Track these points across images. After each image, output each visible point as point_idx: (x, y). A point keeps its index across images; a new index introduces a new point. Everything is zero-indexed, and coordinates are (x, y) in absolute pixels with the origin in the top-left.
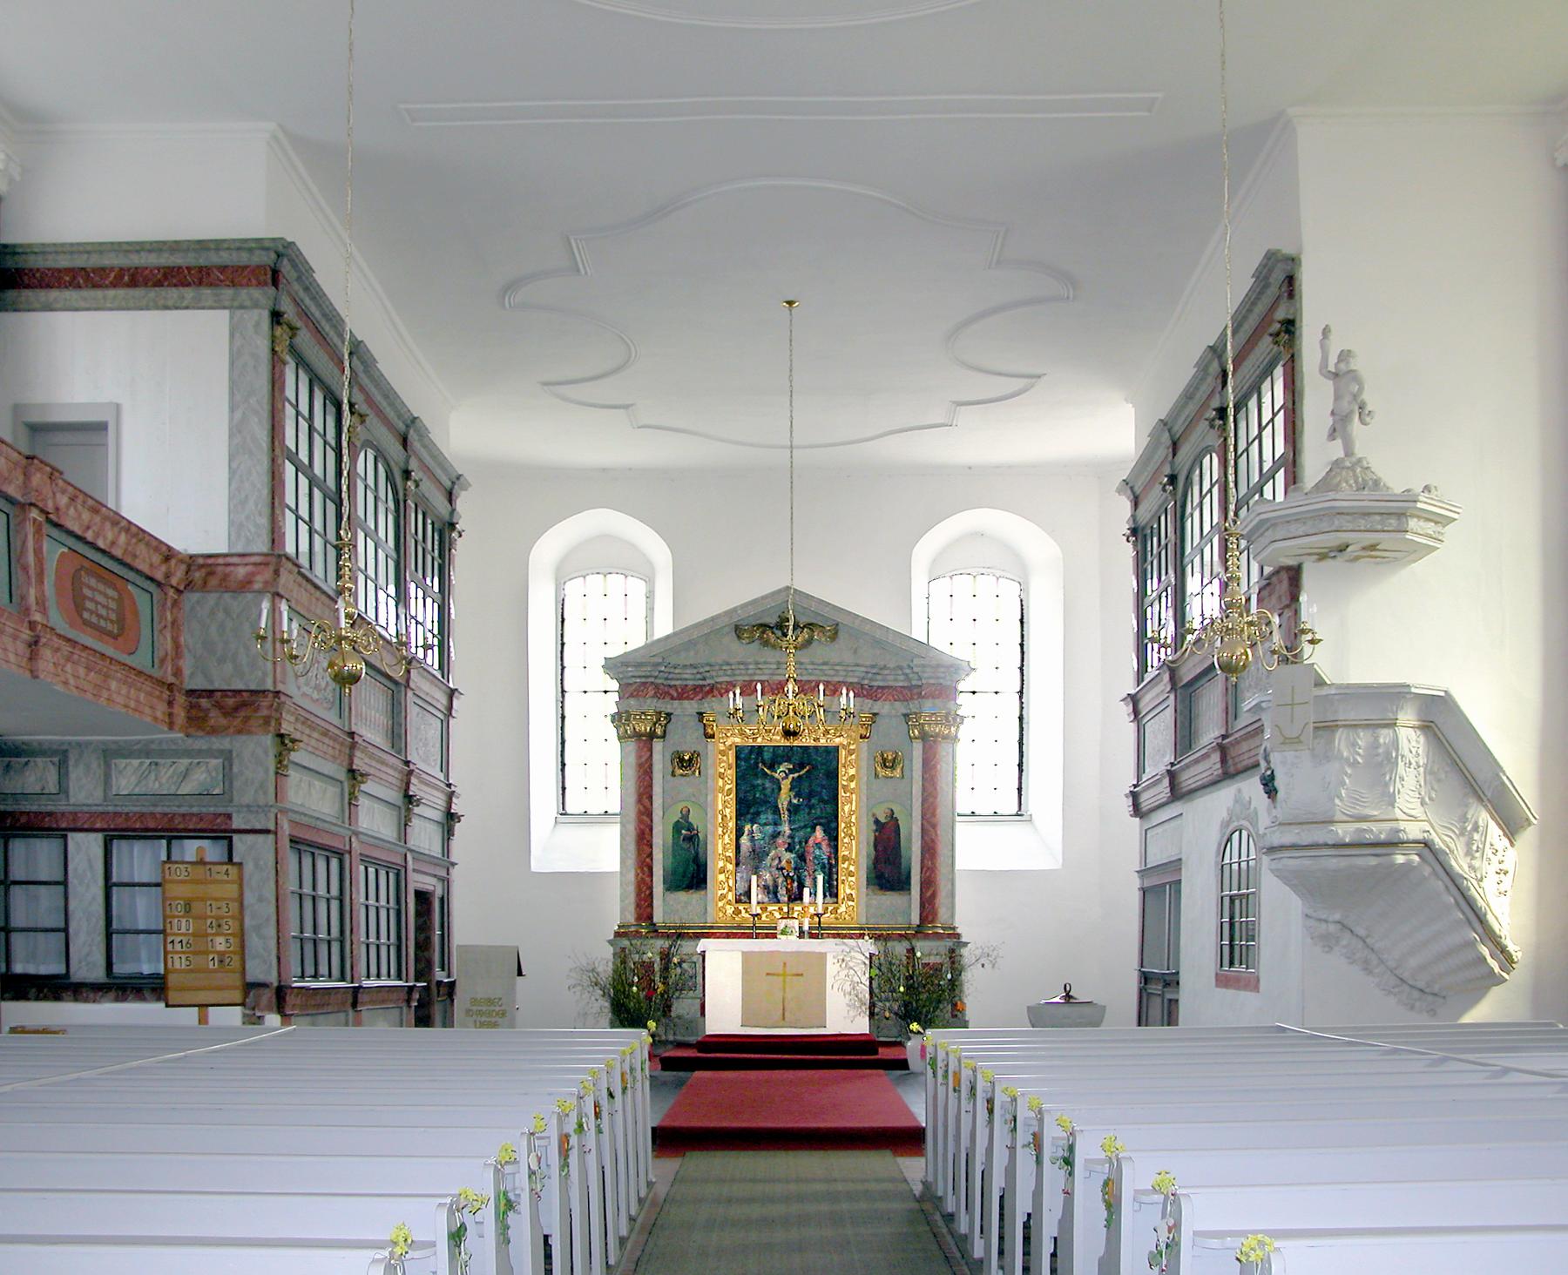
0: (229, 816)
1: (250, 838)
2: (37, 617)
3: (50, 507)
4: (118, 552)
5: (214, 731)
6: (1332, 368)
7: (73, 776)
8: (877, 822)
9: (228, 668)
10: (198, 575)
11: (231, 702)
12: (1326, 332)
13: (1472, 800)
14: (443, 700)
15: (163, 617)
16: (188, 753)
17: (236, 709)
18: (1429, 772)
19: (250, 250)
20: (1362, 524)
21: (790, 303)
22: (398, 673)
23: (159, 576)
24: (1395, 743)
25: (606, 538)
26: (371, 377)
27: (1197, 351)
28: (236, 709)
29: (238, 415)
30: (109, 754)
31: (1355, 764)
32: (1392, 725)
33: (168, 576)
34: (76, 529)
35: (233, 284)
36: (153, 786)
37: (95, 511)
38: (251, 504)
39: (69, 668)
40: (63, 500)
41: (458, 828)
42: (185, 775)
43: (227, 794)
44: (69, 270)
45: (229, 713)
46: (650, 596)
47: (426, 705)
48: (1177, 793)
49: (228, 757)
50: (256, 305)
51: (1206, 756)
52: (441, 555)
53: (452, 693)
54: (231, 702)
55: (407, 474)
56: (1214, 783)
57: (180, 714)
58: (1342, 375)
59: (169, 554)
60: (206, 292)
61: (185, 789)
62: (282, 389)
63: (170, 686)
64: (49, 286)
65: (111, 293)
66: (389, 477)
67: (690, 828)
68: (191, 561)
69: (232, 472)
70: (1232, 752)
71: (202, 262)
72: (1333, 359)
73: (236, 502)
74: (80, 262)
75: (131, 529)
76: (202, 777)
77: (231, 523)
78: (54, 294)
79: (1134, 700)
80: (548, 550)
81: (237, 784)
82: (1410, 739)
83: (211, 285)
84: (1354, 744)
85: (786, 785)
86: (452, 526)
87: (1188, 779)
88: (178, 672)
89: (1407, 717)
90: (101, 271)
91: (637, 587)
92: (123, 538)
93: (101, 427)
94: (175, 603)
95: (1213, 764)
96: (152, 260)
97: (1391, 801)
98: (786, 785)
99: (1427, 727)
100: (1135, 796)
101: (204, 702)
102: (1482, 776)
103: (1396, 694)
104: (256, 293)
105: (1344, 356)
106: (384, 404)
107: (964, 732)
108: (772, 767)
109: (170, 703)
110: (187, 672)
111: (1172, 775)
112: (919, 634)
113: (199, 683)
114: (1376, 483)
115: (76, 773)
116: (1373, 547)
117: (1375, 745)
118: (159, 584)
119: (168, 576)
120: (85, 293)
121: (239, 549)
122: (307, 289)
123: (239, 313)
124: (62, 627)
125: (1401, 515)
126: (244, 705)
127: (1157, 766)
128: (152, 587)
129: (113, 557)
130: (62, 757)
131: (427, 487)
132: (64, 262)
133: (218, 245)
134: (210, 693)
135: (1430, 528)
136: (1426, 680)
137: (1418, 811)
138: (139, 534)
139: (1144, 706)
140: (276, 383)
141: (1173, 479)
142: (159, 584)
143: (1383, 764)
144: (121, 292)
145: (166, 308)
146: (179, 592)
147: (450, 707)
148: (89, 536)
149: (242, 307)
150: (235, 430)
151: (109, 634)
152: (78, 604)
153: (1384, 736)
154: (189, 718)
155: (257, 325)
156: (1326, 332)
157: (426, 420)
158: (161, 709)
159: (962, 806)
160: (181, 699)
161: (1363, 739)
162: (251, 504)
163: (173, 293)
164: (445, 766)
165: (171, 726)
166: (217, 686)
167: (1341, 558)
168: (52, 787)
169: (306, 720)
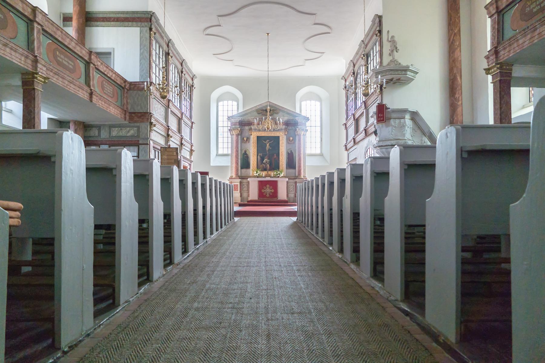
0: (139, 141)
1: (143, 146)
2: (92, 88)
3: (96, 64)
4: (113, 78)
5: (136, 122)
6: (389, 40)
7: (102, 132)
8: (288, 153)
9: (139, 107)
10: (132, 87)
11: (139, 115)
12: (388, 32)
13: (423, 136)
14: (190, 124)
15: (124, 95)
16: (129, 127)
17: (141, 116)
18: (413, 129)
19: (144, 14)
20: (396, 73)
21: (268, 34)
22: (179, 115)
23: (123, 86)
24: (405, 122)
25: (228, 93)
26: (173, 48)
27: (359, 42)
28: (141, 116)
29: (142, 51)
30: (111, 127)
31: (395, 127)
32: (404, 118)
33: (125, 86)
34: (102, 71)
35: (141, 21)
36: (121, 134)
37: (107, 67)
38: (145, 71)
39: (100, 101)
40: (99, 64)
41: (193, 153)
42: (129, 132)
43: (138, 136)
44: (102, 18)
45: (140, 117)
46: (238, 105)
47: (186, 124)
48: (355, 143)
49: (138, 127)
50: (146, 26)
51: (362, 133)
52: (190, 100)
53: (192, 123)
54: (139, 115)
55: (182, 72)
56: (364, 139)
57: (128, 118)
58: (393, 41)
59: (125, 81)
60: (134, 23)
61: (129, 134)
62: (152, 46)
63: (125, 111)
64: (97, 21)
65: (112, 23)
66: (178, 72)
67: (246, 154)
68: (131, 83)
69: (140, 64)
70: (367, 130)
71: (133, 16)
72: (390, 38)
73: (141, 70)
74: (105, 16)
75: (116, 73)
76: (132, 132)
77: (140, 75)
78: (98, 23)
79: (345, 124)
80: (215, 95)
81: (141, 134)
82: (408, 122)
83: (136, 22)
84: (395, 122)
85: (268, 145)
86: (193, 86)
87: (358, 139)
88: (127, 108)
89: (408, 116)
90: (110, 18)
91: (235, 103)
92: (114, 75)
93: (110, 53)
94: (127, 92)
95: (363, 134)
96: (122, 16)
97: (404, 135)
98: (268, 145)
99: (412, 119)
100: (346, 146)
101: (133, 115)
102: (426, 131)
103: (405, 111)
104: (146, 24)
105: (393, 37)
106: (177, 55)
107: (308, 134)
108: (265, 141)
109: (125, 115)
110: (129, 108)
111: (354, 139)
112: (298, 111)
113: (132, 111)
114: (400, 64)
115: (102, 132)
116: (399, 79)
117: (400, 122)
118: (123, 88)
119: (125, 86)
120: (106, 23)
121: (142, 81)
122: (158, 25)
123: (142, 28)
124: (98, 92)
125: (406, 70)
126: (143, 115)
127: (350, 138)
128: (121, 88)
129: (111, 79)
130: (99, 127)
131: (187, 76)
132: (101, 16)
133: (137, 12)
134: (134, 113)
135: (412, 74)
136: (412, 108)
137: (411, 138)
138: (118, 75)
139: (347, 126)
140: (150, 43)
141: (354, 73)
142: (123, 88)
143: (402, 127)
144: (114, 23)
145: (125, 27)
146: (128, 90)
147: (192, 126)
148: (106, 73)
149: (143, 27)
150: (141, 54)
151: (110, 97)
152: (103, 88)
153: (402, 120)
154: (130, 118)
155: (146, 31)
156: (388, 32)
157: (187, 60)
158: (123, 116)
159: (308, 151)
160: (127, 114)
161: (397, 121)
162: (145, 71)
163: (126, 23)
164: (191, 139)
165: (125, 120)
166: (136, 111)
167: (392, 82)
168: (97, 134)
169: (157, 120)
